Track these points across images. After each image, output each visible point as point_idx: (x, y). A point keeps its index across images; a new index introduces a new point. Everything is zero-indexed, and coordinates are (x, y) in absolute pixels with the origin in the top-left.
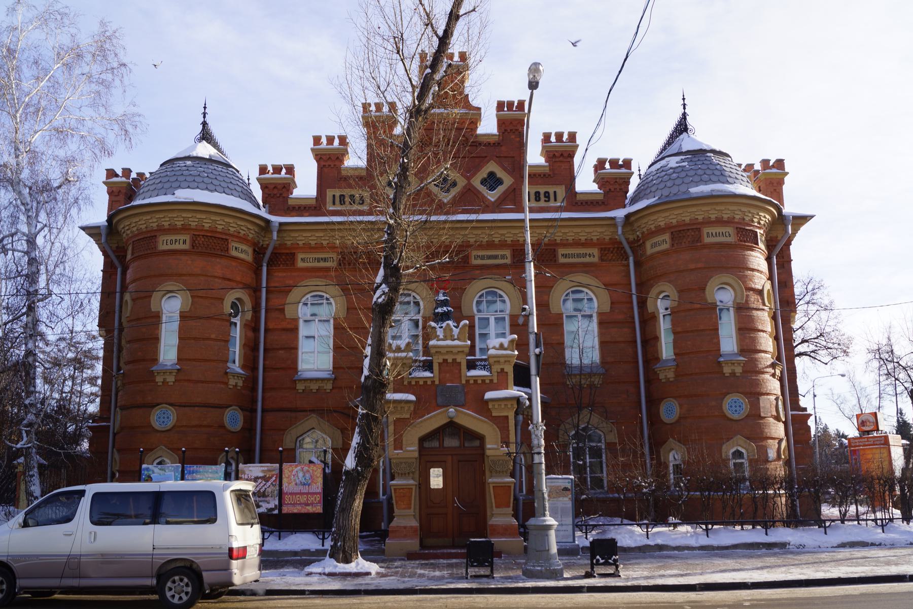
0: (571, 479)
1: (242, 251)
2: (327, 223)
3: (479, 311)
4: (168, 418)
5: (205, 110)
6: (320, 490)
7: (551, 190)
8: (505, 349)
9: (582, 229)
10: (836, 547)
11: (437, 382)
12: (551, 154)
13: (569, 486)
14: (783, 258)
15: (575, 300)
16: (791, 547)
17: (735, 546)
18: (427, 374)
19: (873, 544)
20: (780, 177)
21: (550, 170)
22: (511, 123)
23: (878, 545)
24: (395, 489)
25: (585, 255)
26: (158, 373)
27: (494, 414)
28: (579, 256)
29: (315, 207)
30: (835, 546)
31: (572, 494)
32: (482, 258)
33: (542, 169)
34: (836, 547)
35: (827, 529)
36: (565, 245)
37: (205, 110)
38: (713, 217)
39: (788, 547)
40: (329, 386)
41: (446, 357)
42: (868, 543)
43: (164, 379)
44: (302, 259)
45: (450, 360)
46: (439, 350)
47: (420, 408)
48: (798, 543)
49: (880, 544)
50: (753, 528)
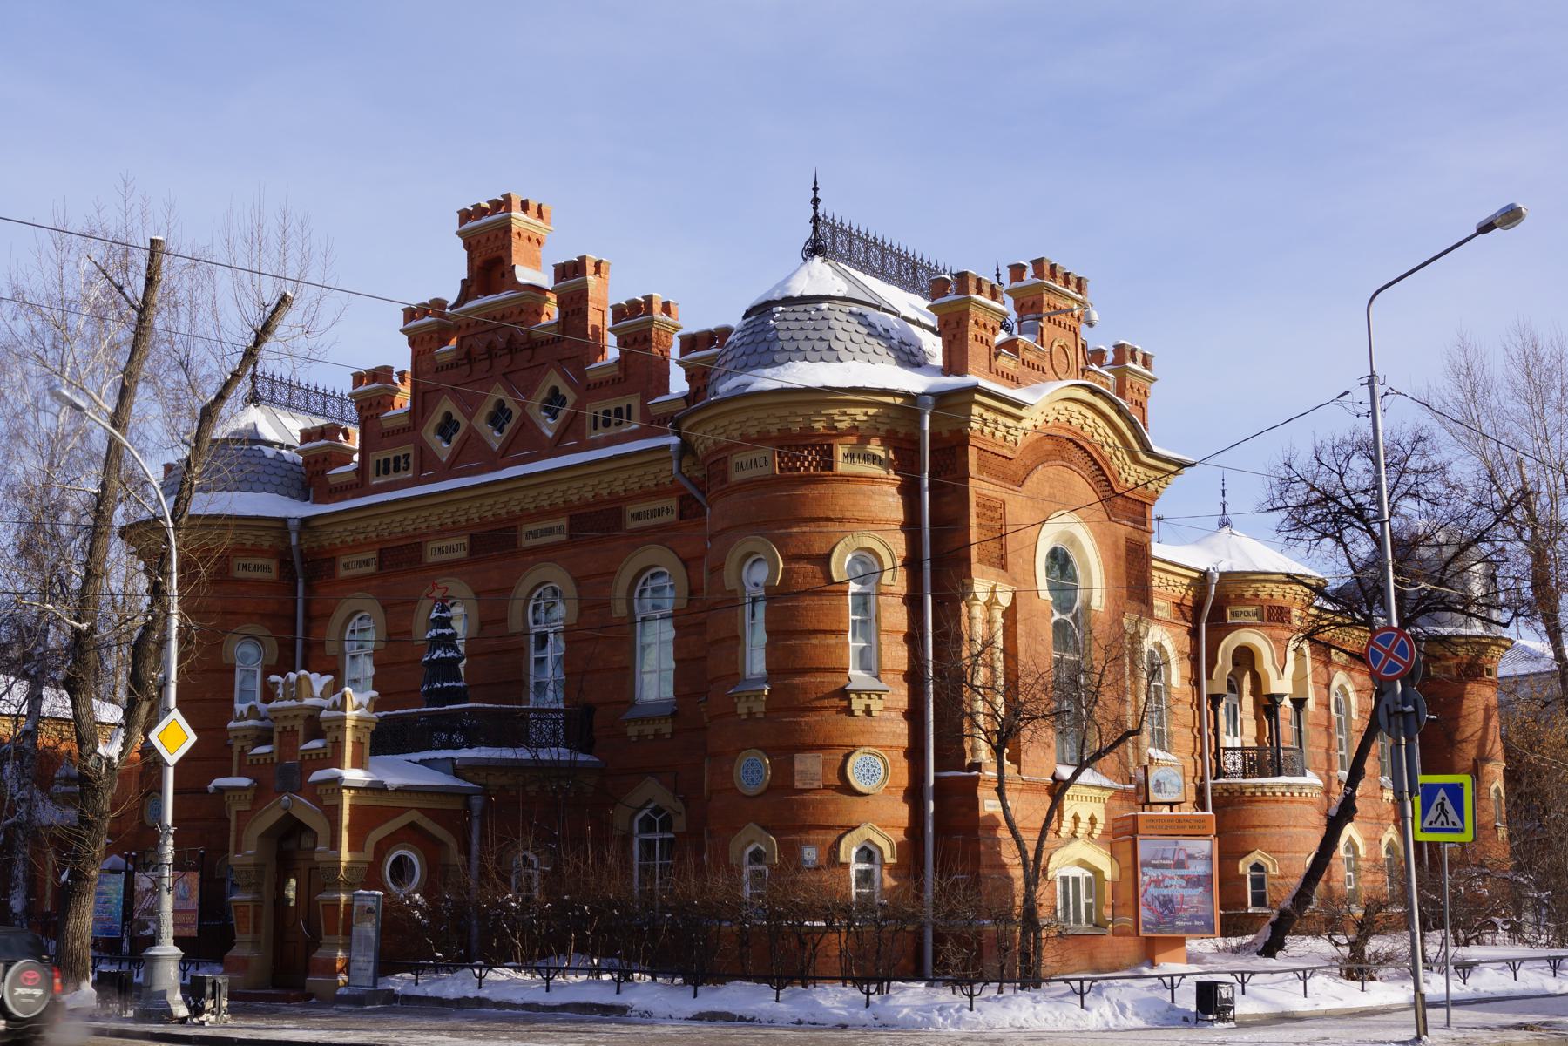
0: (378, 896)
1: (256, 568)
2: (397, 501)
3: (536, 622)
4: (758, 772)
5: (815, 193)
6: (195, 907)
7: (622, 403)
8: (246, 719)
9: (495, 499)
10: (691, 1019)
11: (275, 760)
12: (366, 405)
13: (372, 905)
14: (956, 472)
15: (654, 590)
16: (633, 1014)
17: (564, 1007)
18: (265, 749)
19: (741, 1019)
20: (961, 308)
21: (620, 369)
22: (572, 299)
23: (748, 1021)
24: (323, 905)
25: (654, 513)
26: (738, 697)
27: (326, 803)
28: (654, 513)
29: (357, 484)
30: (689, 1016)
31: (377, 918)
32: (549, 531)
33: (608, 370)
34: (691, 1019)
35: (975, 998)
36: (634, 499)
37: (815, 193)
38: (752, 432)
39: (629, 1012)
40: (667, 729)
41: (285, 724)
42: (735, 1016)
43: (749, 708)
44: (345, 565)
45: (289, 729)
46: (286, 713)
47: (260, 795)
48: (643, 1009)
49: (752, 1020)
50: (654, 979)
